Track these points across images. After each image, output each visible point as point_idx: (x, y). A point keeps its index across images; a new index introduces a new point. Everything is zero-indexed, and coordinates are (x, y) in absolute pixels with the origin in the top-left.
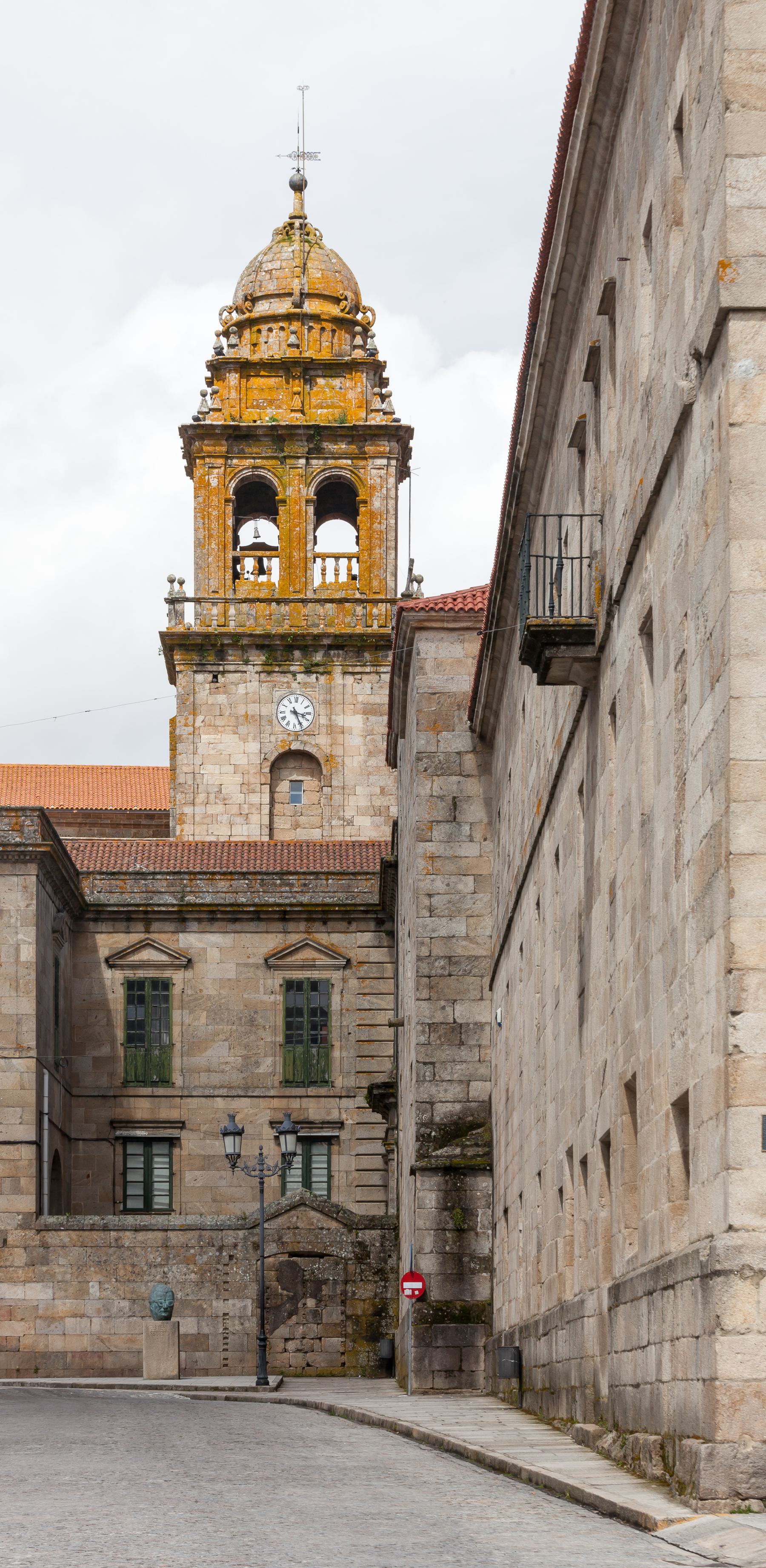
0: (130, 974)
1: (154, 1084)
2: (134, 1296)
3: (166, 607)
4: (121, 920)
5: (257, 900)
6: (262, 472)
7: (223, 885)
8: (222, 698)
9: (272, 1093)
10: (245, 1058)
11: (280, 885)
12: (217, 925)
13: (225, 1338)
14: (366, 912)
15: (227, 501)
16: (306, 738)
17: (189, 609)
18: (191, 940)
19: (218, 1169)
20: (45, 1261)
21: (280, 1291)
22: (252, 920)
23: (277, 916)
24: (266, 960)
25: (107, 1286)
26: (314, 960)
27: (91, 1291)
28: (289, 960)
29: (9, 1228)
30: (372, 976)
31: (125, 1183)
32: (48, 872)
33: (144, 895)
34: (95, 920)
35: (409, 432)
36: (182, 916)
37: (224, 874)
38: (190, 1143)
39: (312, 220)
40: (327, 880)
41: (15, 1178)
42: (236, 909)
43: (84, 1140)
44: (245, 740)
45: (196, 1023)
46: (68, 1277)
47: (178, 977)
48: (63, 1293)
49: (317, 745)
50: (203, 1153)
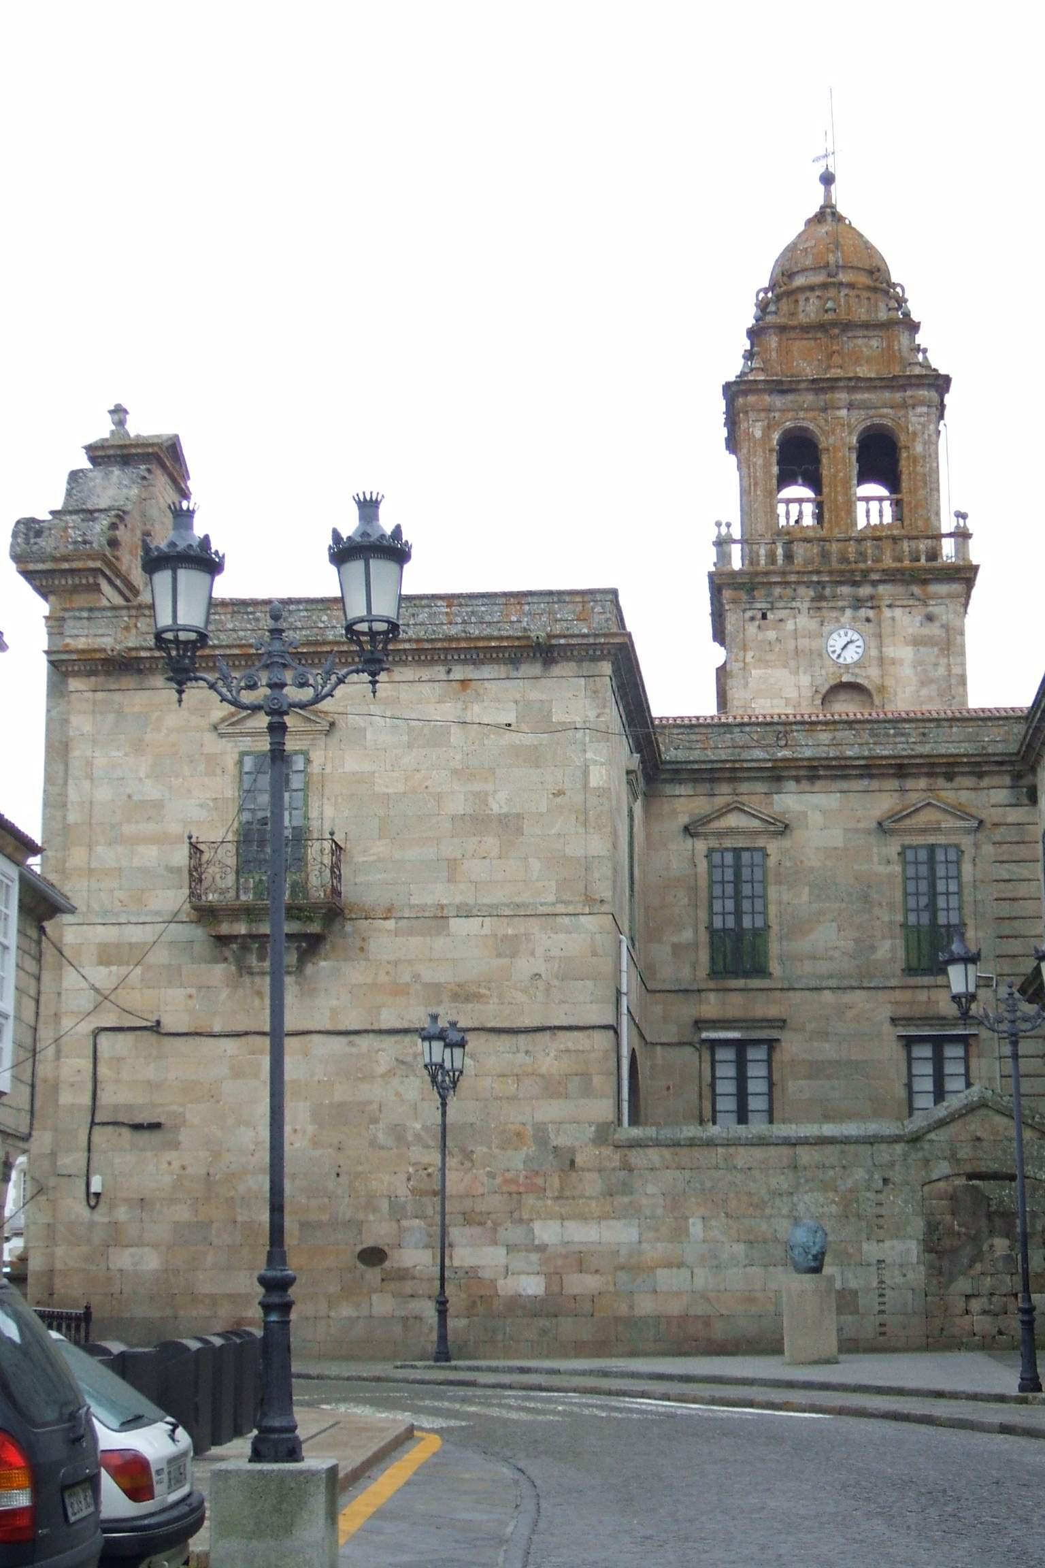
0: (714, 843)
1: (747, 975)
2: (751, 1237)
3: (714, 550)
4: (704, 780)
5: (866, 753)
6: (805, 424)
7: (825, 737)
8: (771, 635)
9: (893, 983)
10: (857, 941)
11: (895, 735)
12: (819, 785)
13: (882, 1295)
14: (1001, 763)
15: (771, 450)
16: (857, 670)
17: (736, 550)
18: (791, 801)
19: (829, 1078)
20: (627, 1189)
21: (956, 1227)
22: (861, 776)
23: (892, 771)
24: (880, 824)
25: (713, 1223)
26: (939, 822)
27: (692, 1230)
28: (907, 823)
29: (577, 1144)
30: (1009, 839)
31: (714, 1094)
32: (623, 684)
33: (729, 751)
34: (672, 781)
35: (941, 383)
36: (776, 774)
37: (826, 723)
38: (792, 1046)
39: (841, 210)
40: (951, 727)
41: (585, 1075)
42: (843, 763)
43: (662, 1044)
44: (796, 673)
45: (795, 902)
46: (659, 1212)
47: (773, 847)
48: (651, 1235)
49: (867, 677)
50: (809, 1058)
